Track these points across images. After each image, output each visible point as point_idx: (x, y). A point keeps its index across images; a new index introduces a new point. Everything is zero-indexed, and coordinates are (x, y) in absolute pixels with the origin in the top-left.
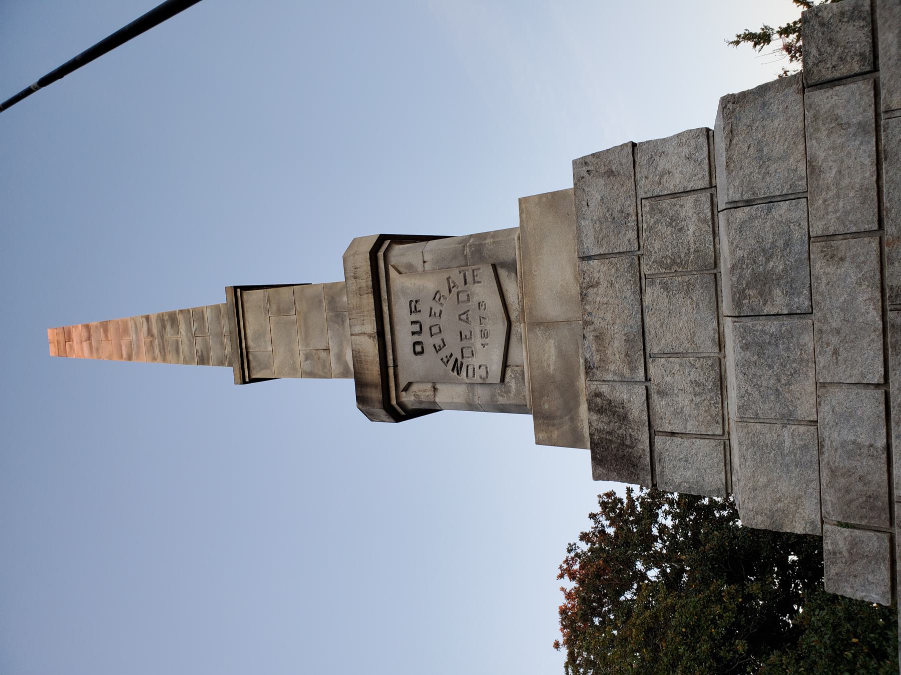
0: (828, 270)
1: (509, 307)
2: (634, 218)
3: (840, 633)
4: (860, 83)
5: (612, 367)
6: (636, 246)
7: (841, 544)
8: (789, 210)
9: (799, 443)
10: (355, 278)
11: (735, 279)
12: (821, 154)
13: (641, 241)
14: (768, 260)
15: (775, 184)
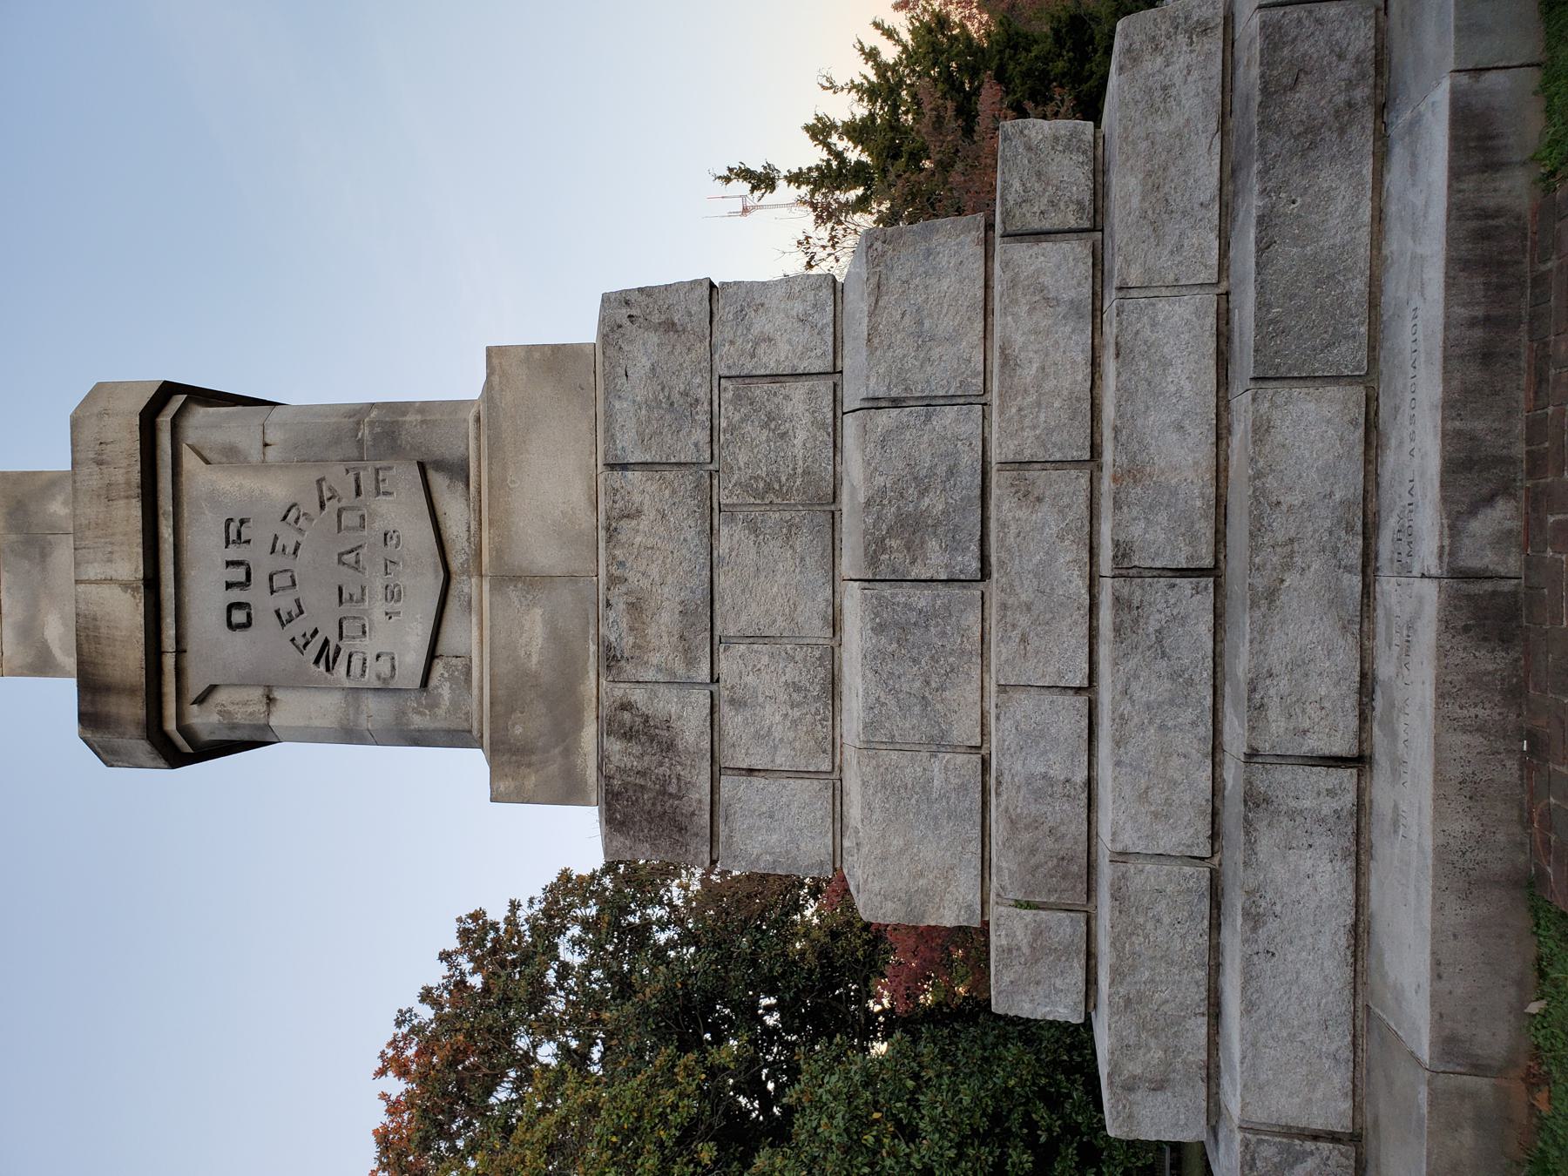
0: (1019, 514)
1: (448, 547)
2: (706, 407)
3: (857, 1108)
4: (1075, 244)
5: (655, 659)
6: (707, 456)
7: (1020, 934)
8: (957, 420)
9: (955, 781)
10: (100, 463)
11: (870, 521)
12: (1019, 339)
13: (716, 447)
14: (922, 494)
15: (939, 376)
